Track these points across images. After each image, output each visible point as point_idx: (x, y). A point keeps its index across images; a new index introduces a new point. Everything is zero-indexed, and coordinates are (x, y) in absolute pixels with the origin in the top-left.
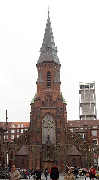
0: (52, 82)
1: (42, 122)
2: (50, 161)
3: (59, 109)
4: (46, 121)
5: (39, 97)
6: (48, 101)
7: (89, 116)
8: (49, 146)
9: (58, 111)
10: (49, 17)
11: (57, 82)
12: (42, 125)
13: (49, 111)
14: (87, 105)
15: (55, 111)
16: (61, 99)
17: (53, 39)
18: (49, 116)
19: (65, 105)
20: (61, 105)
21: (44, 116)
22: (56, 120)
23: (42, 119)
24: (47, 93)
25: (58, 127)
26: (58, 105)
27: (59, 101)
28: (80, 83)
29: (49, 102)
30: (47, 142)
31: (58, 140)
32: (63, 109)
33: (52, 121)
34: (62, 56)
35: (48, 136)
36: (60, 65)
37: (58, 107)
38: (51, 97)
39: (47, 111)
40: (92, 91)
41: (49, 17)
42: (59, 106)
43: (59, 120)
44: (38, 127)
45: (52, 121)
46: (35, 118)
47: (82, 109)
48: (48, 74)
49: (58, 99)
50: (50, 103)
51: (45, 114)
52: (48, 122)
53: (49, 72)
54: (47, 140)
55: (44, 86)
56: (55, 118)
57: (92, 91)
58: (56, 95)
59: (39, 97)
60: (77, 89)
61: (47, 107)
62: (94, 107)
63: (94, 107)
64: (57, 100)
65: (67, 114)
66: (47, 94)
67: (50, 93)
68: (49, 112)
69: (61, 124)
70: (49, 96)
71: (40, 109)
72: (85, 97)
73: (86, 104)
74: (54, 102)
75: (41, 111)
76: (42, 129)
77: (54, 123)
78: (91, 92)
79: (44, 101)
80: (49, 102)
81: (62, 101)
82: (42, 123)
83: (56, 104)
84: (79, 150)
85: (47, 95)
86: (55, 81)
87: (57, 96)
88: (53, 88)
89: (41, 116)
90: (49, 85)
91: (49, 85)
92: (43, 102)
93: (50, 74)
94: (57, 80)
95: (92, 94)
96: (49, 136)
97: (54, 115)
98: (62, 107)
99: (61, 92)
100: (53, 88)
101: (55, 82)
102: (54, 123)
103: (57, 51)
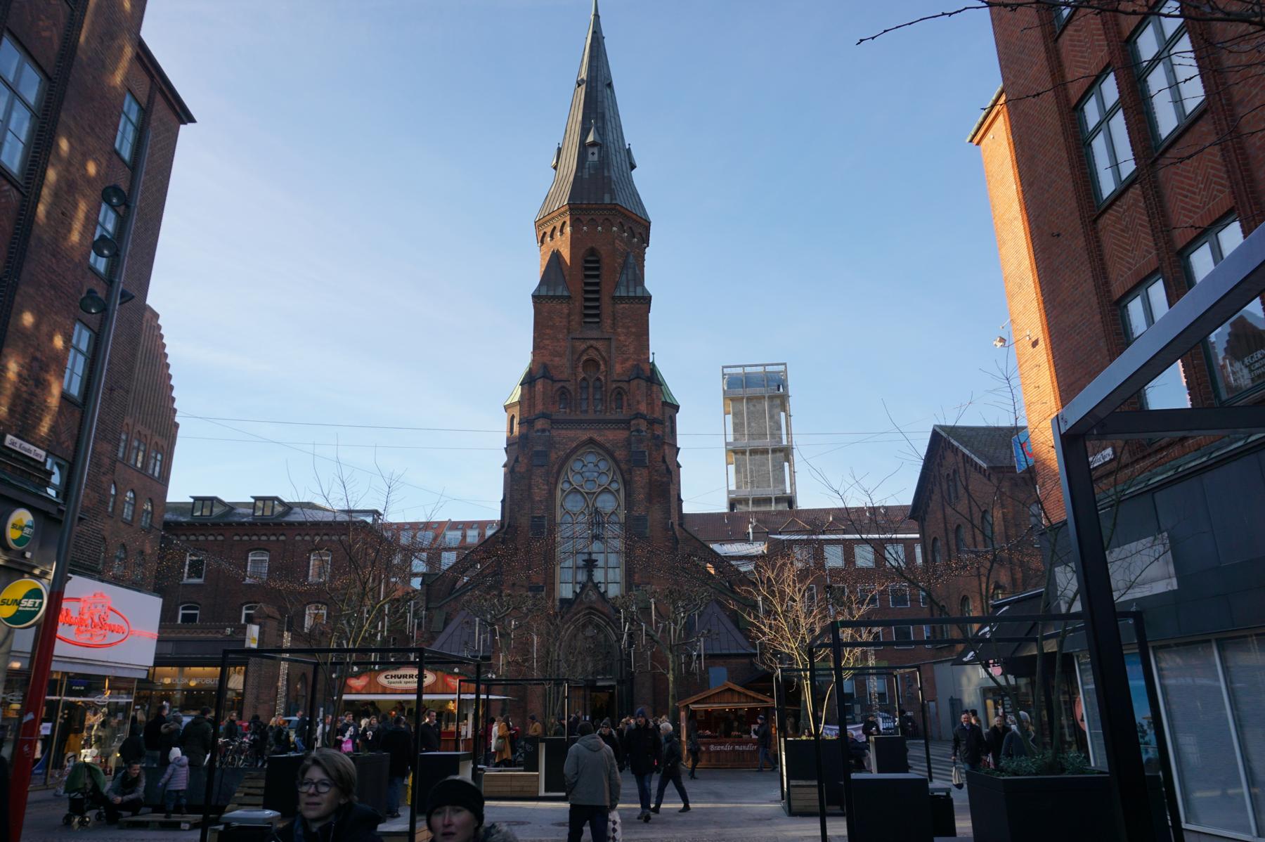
0: (606, 299)
1: (560, 486)
2: (599, 684)
3: (643, 425)
4: (576, 480)
5: (545, 366)
6: (587, 387)
7: (767, 501)
8: (592, 609)
9: (638, 431)
10: (597, 16)
11: (629, 298)
12: (558, 502)
13: (596, 436)
14: (758, 457)
15: (621, 435)
16: (652, 378)
17: (619, 127)
18: (591, 458)
19: (668, 410)
20: (651, 404)
21: (568, 456)
22: (626, 476)
23: (559, 473)
24: (583, 346)
25: (639, 511)
26: (638, 402)
27: (643, 383)
28: (727, 371)
29: (591, 390)
30: (582, 589)
31: (636, 576)
32: (662, 423)
33: (604, 480)
34: (652, 185)
35: (586, 557)
36: (645, 226)
37: (639, 416)
38: (602, 367)
39: (584, 436)
40: (778, 401)
41: (597, 16)
42: (643, 408)
43: (641, 477)
44: (538, 513)
45: (604, 480)
46: (523, 470)
47: (738, 471)
48: (587, 262)
49: (638, 377)
50: (598, 397)
51: (574, 451)
52: (588, 487)
53: (593, 251)
54: (582, 577)
55: (569, 315)
56: (623, 466)
57: (778, 401)
58: (627, 360)
59: (545, 366)
60: (719, 386)
61: (583, 417)
62: (786, 464)
63: (786, 464)
64: (634, 383)
65: (679, 459)
66: (581, 355)
67: (596, 349)
68: (591, 441)
69: (650, 499)
70: (592, 363)
71: (547, 426)
72: (749, 424)
73: (754, 452)
74: (620, 393)
75: (554, 433)
76: (558, 519)
77: (618, 491)
78: (771, 407)
79: (571, 388)
80: (591, 390)
81: (655, 388)
82: (559, 493)
83: (625, 398)
84: (568, 767)
85: (585, 358)
86: (624, 294)
87: (629, 364)
88: (614, 326)
89: (553, 456)
90: (591, 310)
91: (591, 310)
92: (563, 392)
93: (597, 262)
94: (631, 289)
95: (776, 411)
96: (594, 556)
97: (617, 454)
98: (657, 415)
99: (651, 351)
100: (614, 326)
101: (621, 298)
102: (618, 491)
103: (633, 167)
